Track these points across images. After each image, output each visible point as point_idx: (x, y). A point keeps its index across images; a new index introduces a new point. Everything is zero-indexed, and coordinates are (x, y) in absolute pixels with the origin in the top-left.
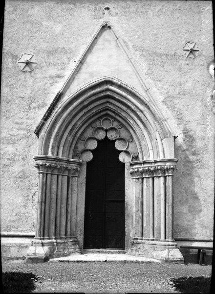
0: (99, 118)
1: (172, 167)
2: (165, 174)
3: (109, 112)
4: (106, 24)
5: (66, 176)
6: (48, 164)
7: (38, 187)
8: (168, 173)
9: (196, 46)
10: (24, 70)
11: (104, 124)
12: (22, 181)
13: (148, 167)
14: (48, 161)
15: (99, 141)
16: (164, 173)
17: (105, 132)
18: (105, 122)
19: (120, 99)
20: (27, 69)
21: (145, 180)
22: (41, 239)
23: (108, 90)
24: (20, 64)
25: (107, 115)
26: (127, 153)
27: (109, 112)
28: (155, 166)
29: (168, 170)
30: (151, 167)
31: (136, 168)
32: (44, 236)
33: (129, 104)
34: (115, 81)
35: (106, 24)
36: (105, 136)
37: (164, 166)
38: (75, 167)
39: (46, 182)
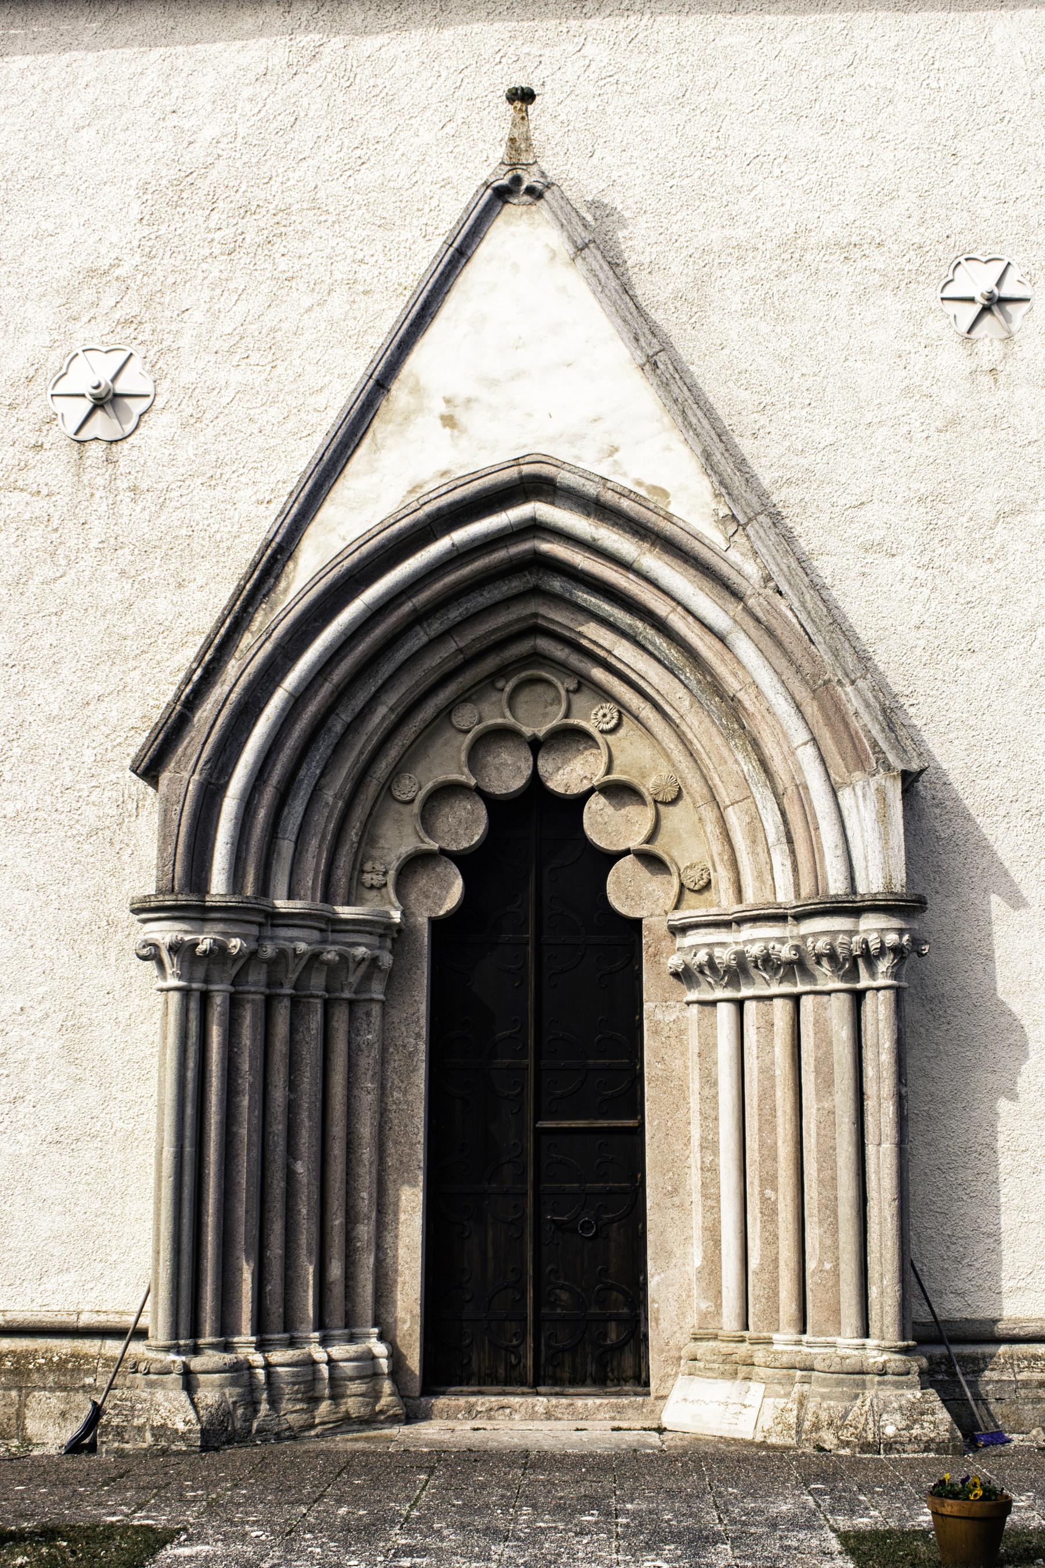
0: (491, 680)
1: (891, 939)
2: (857, 979)
3: (544, 644)
4: (517, 180)
5: (317, 997)
6: (204, 945)
7: (155, 1050)
8: (873, 975)
9: (1013, 275)
10: (80, 437)
11: (521, 712)
12: (790, 1428)
13: (767, 940)
14: (209, 927)
15: (494, 804)
16: (853, 974)
17: (527, 754)
18: (524, 697)
19: (214, 1074)
20: (101, 425)
21: (750, 1007)
22: (178, 1350)
23: (534, 528)
24: (61, 405)
25: (538, 658)
26: (653, 862)
27: (544, 644)
28: (804, 938)
29: (869, 958)
30: (782, 941)
31: (698, 947)
32: (195, 1332)
33: (660, 606)
34: (565, 478)
35: (517, 180)
36: (527, 772)
37: (851, 933)
38: (361, 951)
39: (274, 630)
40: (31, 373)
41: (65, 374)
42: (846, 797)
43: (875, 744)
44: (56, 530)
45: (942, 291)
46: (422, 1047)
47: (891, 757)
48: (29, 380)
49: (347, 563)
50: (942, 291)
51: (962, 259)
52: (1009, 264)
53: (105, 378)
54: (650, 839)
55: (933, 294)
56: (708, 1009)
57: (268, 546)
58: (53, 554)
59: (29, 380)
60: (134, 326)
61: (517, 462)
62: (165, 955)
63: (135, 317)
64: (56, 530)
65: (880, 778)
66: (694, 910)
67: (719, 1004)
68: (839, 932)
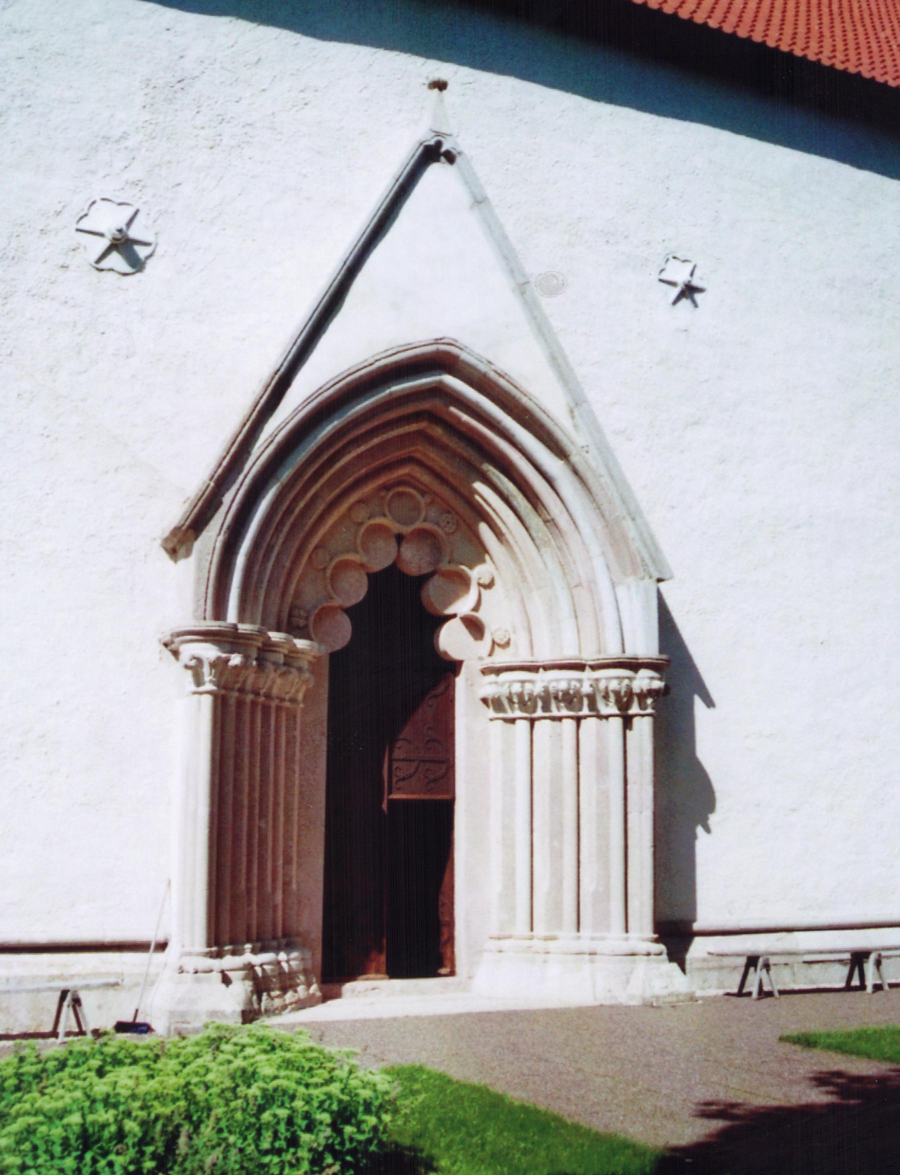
17: (393, 542)
40: (59, 208)
41: (86, 215)
42: (621, 591)
43: (643, 560)
44: (80, 334)
45: (78, 221)
46: (325, 741)
47: (652, 569)
48: (58, 213)
49: (326, 394)
50: (78, 221)
51: (670, 257)
52: (137, 213)
53: (122, 225)
54: (476, 608)
55: (655, 276)
56: (557, 723)
57: (276, 373)
58: (79, 353)
59: (58, 213)
60: (139, 188)
61: (437, 341)
62: (206, 669)
63: (140, 181)
64: (80, 334)
65: (647, 580)
66: (501, 658)
67: (518, 722)
68: (624, 678)
